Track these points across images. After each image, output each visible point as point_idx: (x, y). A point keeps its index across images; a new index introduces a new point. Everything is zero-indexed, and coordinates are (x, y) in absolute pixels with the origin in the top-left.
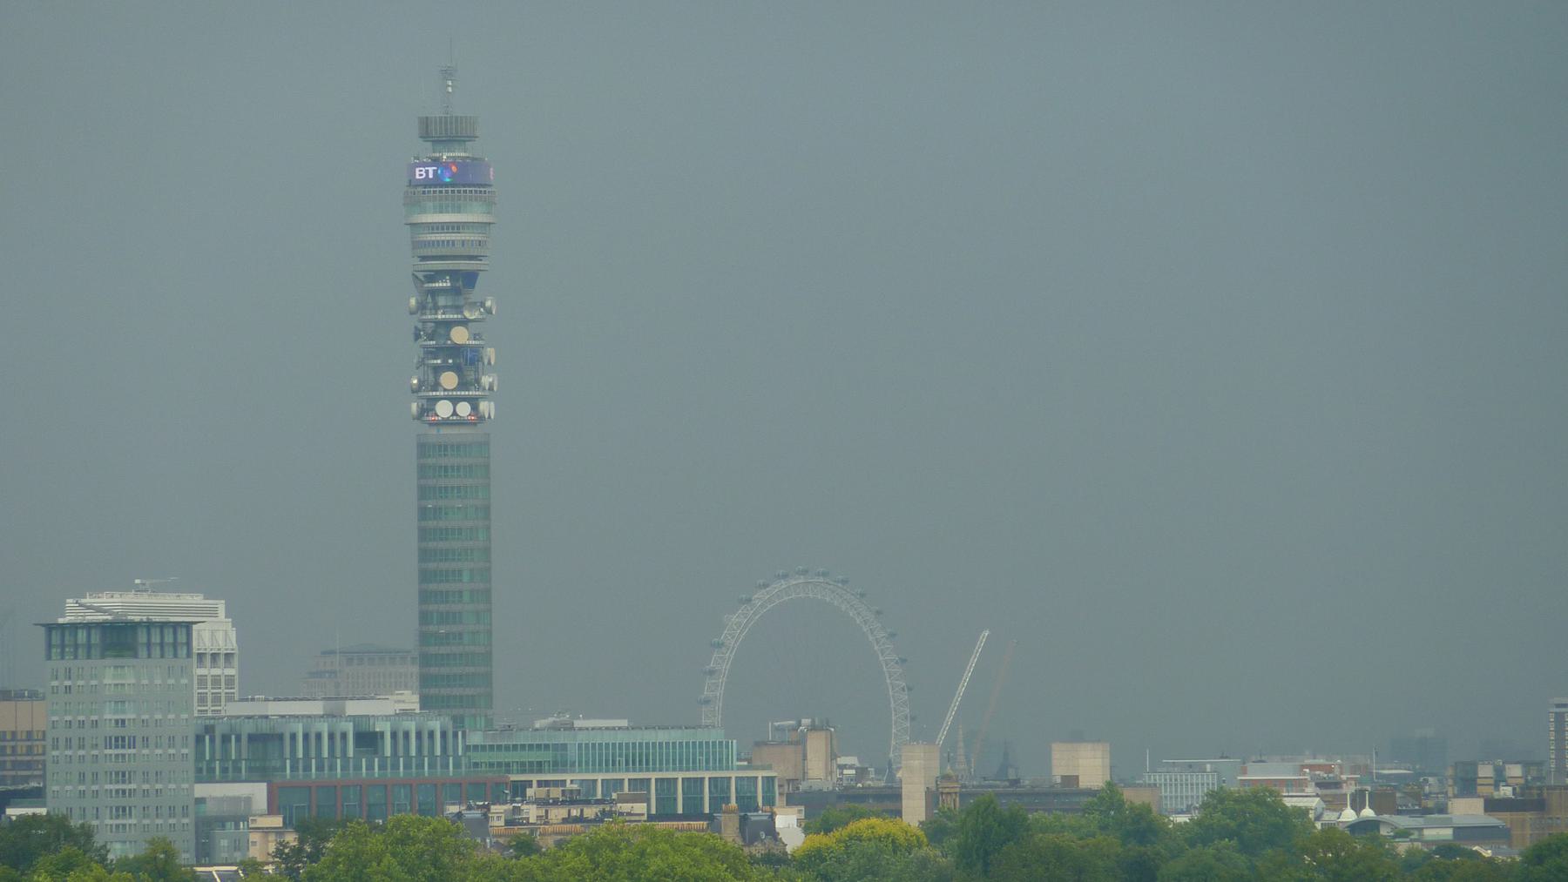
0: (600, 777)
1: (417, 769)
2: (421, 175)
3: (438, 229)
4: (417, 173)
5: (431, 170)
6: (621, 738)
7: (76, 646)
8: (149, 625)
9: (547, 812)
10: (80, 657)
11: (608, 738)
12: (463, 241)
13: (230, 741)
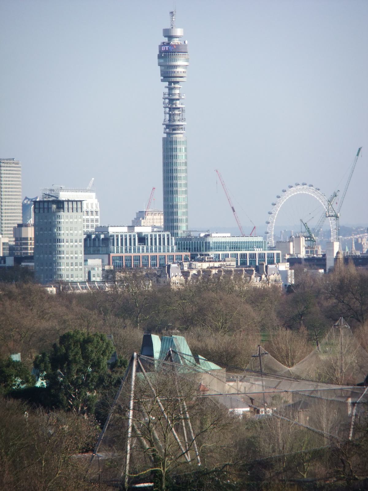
0: (221, 253)
4: (162, 48)
5: (167, 47)
6: (228, 240)
7: (44, 208)
8: (68, 201)
9: (202, 265)
11: (223, 240)
13: (87, 241)
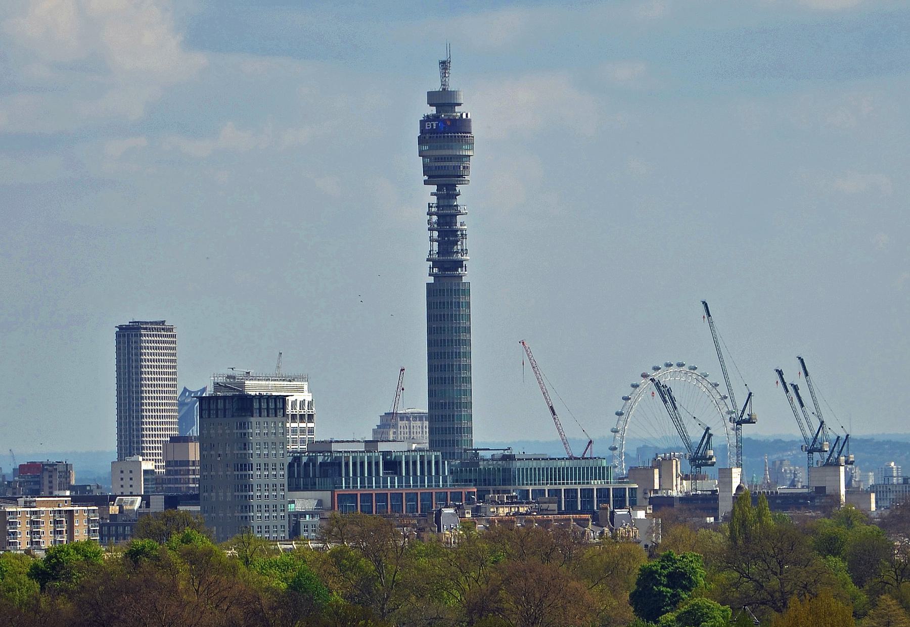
1: (435, 483)
2: (428, 127)
3: (445, 158)
10: (219, 416)
12: (454, 166)
